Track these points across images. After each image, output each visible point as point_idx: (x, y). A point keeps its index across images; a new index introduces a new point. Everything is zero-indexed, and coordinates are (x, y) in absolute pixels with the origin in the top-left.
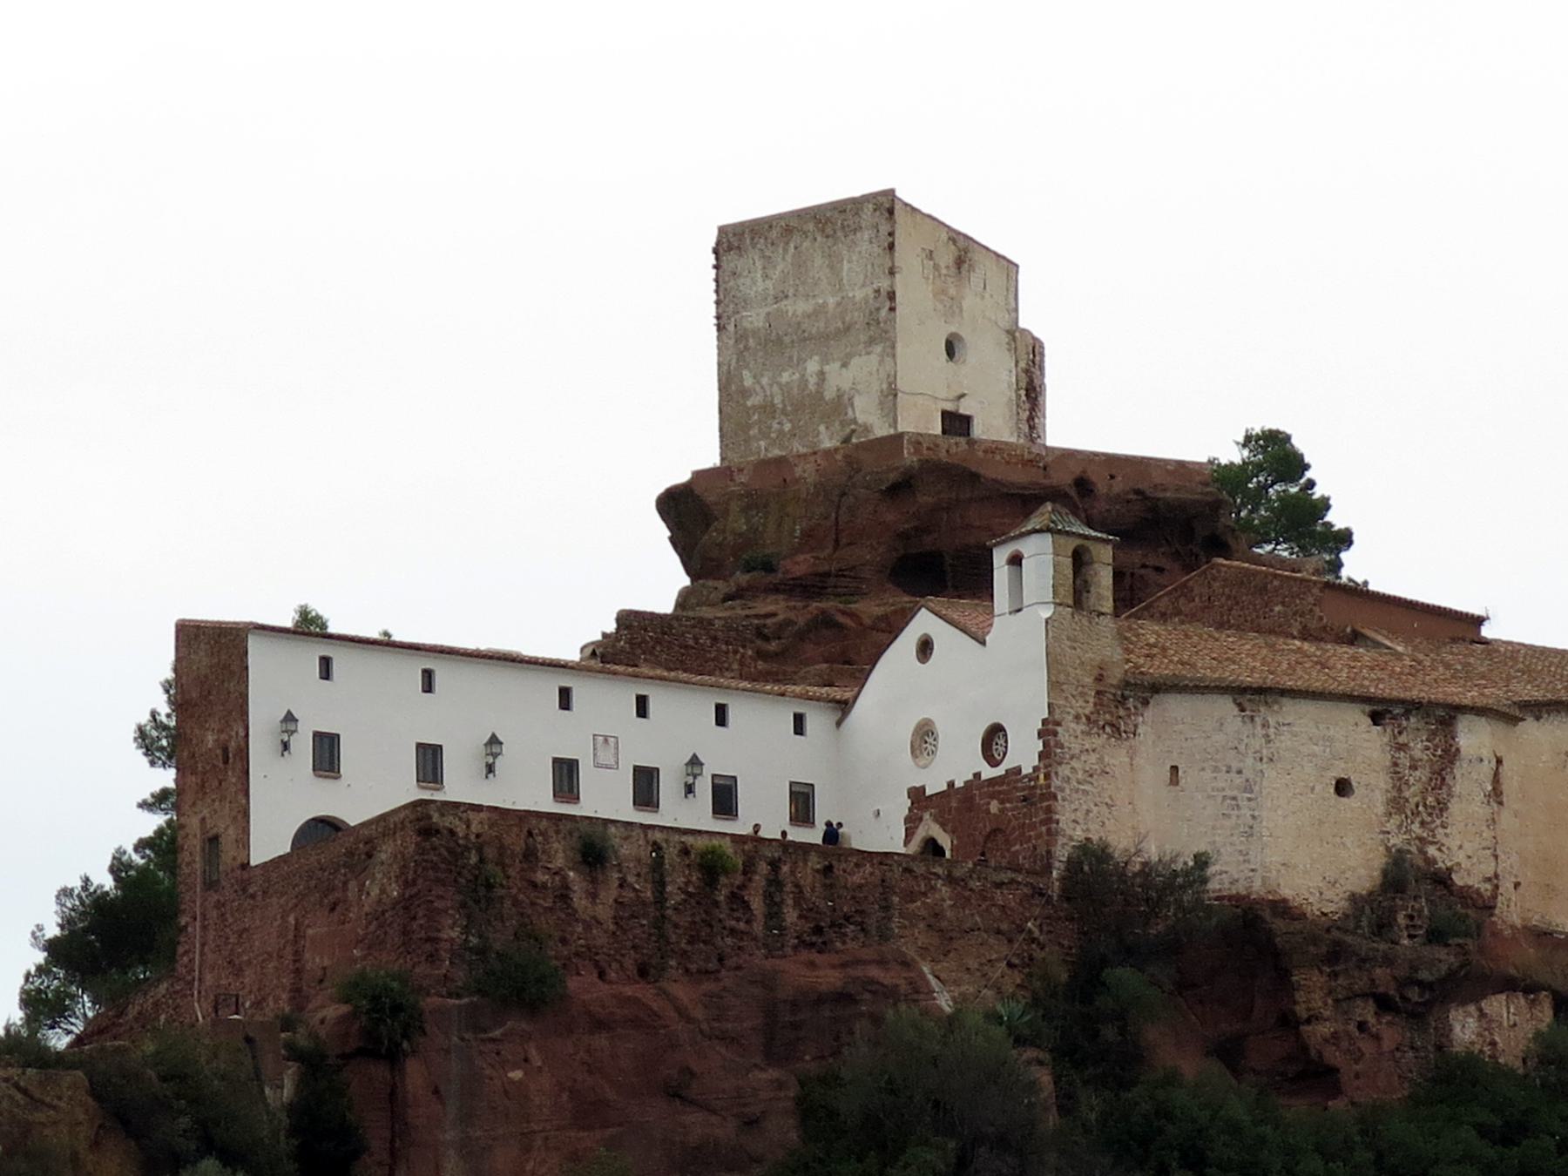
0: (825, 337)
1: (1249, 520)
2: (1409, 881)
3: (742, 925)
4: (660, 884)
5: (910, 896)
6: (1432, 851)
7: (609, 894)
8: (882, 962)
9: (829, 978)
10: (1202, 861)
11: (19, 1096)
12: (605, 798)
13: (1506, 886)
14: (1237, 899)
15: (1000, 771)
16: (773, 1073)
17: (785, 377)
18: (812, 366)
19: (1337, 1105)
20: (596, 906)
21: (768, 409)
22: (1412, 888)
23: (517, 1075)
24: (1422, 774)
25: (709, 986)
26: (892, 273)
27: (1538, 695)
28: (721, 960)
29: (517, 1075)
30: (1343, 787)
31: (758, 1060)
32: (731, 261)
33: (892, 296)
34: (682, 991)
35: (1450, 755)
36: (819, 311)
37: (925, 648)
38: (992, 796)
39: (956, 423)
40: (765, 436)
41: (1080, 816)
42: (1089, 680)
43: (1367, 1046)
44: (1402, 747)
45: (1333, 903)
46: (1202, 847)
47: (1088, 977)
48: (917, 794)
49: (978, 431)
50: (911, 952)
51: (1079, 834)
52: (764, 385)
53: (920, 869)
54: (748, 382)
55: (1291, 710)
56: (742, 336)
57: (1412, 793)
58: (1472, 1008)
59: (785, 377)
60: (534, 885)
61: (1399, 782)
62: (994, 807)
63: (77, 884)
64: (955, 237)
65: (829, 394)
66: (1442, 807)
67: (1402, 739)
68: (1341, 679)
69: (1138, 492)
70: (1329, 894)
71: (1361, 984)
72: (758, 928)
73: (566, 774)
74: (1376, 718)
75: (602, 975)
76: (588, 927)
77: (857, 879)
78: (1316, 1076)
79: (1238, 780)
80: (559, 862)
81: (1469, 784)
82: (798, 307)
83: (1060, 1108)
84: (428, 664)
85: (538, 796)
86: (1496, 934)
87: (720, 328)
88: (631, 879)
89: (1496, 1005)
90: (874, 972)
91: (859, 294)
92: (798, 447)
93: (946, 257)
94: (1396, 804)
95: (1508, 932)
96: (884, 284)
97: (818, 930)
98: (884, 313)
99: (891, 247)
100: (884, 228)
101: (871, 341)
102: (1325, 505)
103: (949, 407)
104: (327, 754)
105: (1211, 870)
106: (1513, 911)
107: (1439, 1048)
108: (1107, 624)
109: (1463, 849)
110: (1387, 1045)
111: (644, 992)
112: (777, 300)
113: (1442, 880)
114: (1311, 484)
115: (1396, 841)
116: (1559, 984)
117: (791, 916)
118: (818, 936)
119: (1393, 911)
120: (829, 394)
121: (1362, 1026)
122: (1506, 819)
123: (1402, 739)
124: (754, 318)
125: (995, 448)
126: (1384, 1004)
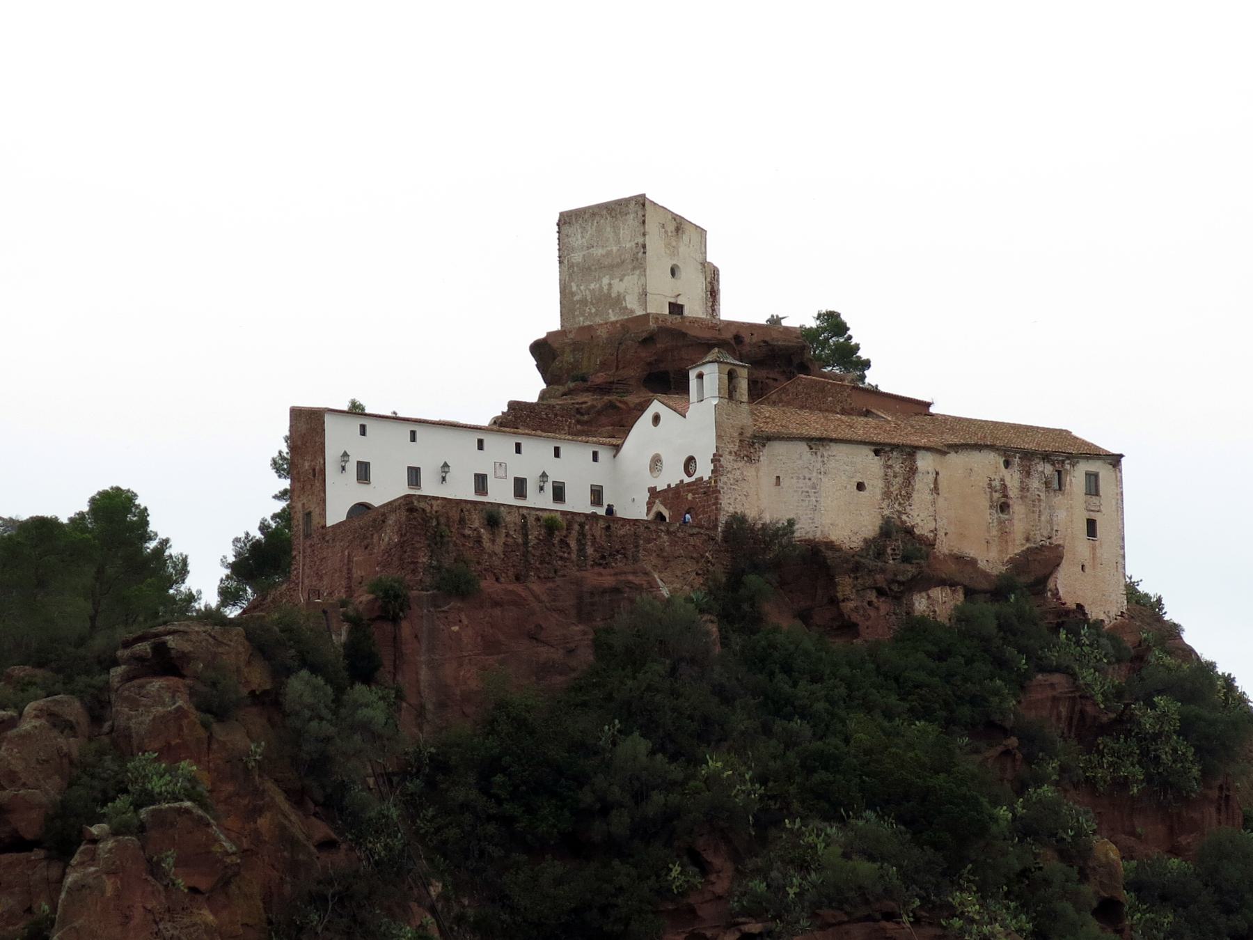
4: (526, 535)
5: (649, 541)
6: (904, 517)
7: (501, 540)
9: (608, 581)
10: (791, 523)
12: (500, 493)
13: (941, 533)
15: (693, 479)
16: (581, 627)
17: (592, 286)
18: (605, 281)
20: (494, 546)
21: (584, 302)
22: (894, 536)
23: (455, 628)
24: (899, 480)
26: (644, 235)
29: (455, 628)
30: (860, 487)
32: (566, 229)
33: (644, 246)
34: (536, 587)
35: (913, 471)
36: (609, 254)
37: (656, 419)
38: (689, 491)
39: (676, 308)
40: (583, 315)
42: (736, 435)
43: (872, 613)
44: (890, 467)
45: (856, 543)
47: (735, 580)
48: (652, 491)
49: (687, 312)
50: (649, 568)
51: (731, 510)
53: (653, 527)
54: (574, 288)
55: (836, 449)
56: (571, 266)
58: (924, 594)
59: (592, 286)
60: (464, 536)
62: (690, 496)
63: (242, 536)
66: (909, 496)
67: (890, 463)
68: (860, 433)
69: (765, 342)
70: (854, 539)
71: (869, 582)
72: (574, 556)
73: (481, 482)
74: (877, 453)
75: (497, 580)
76: (490, 556)
78: (849, 628)
79: (810, 483)
81: (922, 484)
82: (599, 252)
85: (467, 492)
88: (512, 533)
89: (936, 593)
90: (631, 578)
91: (628, 246)
92: (598, 320)
93: (671, 227)
94: (887, 494)
96: (641, 240)
97: (603, 557)
98: (640, 254)
99: (644, 222)
100: (640, 213)
101: (634, 269)
102: (857, 347)
103: (673, 300)
104: (364, 472)
105: (797, 527)
106: (944, 546)
107: (908, 613)
109: (920, 517)
110: (882, 612)
111: (518, 588)
112: (588, 248)
113: (909, 531)
115: (887, 512)
116: (966, 583)
117: (590, 550)
118: (603, 560)
119: (885, 547)
121: (870, 603)
123: (890, 463)
124: (577, 257)
125: (694, 321)
126: (881, 592)
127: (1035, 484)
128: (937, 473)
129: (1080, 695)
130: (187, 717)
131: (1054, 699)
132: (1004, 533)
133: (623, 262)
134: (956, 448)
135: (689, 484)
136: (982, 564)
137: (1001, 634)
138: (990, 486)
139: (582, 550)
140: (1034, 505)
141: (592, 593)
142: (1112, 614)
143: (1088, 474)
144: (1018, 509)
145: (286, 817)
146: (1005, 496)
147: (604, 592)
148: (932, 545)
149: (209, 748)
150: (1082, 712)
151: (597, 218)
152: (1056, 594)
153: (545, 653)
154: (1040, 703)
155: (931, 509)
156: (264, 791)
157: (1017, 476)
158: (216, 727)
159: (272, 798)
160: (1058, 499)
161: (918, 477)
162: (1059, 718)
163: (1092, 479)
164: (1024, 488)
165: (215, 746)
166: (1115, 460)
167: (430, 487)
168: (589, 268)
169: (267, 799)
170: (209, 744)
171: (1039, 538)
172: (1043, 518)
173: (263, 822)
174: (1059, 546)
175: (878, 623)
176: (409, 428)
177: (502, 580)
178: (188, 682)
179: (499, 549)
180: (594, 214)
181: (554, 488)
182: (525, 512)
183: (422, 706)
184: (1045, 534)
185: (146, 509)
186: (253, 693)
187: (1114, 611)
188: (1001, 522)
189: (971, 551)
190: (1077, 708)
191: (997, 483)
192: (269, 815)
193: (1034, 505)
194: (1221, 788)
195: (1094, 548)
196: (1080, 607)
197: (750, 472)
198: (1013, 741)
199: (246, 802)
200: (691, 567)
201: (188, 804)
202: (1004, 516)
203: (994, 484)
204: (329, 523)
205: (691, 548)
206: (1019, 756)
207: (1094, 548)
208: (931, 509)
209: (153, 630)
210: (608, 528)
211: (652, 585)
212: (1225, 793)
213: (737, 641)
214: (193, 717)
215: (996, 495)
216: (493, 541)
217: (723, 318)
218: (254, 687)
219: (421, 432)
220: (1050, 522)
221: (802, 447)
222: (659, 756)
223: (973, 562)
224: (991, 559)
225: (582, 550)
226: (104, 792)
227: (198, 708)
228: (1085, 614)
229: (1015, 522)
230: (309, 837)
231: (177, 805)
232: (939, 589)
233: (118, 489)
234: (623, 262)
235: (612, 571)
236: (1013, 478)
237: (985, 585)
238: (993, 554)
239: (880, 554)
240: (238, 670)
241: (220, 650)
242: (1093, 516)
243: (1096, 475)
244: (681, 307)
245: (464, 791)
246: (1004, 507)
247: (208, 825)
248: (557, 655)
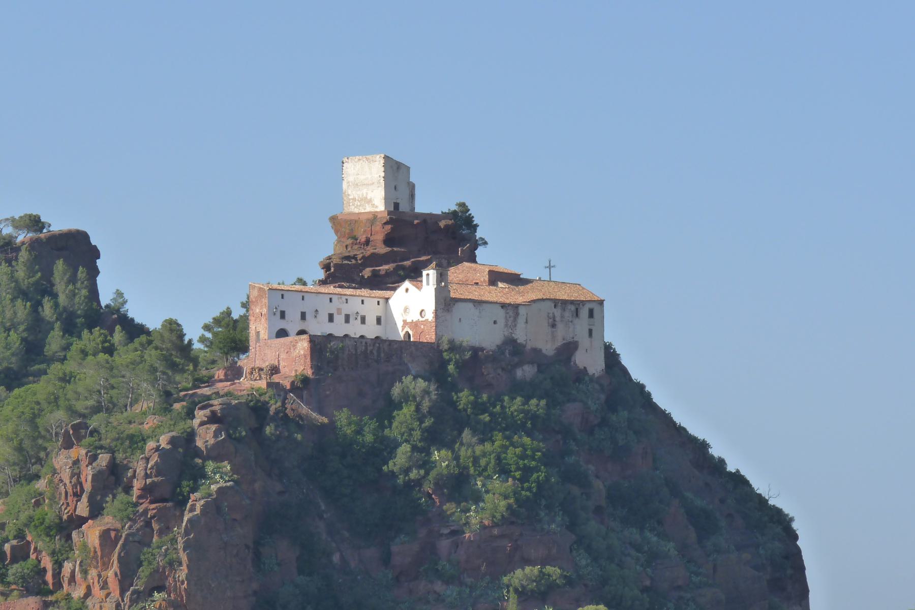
0: (368, 185)
1: (539, 400)
2: (510, 342)
4: (356, 350)
21: (354, 199)
30: (495, 322)
37: (407, 290)
45: (494, 347)
55: (484, 305)
64: (397, 163)
66: (515, 326)
82: (362, 177)
94: (506, 325)
109: (520, 335)
115: (506, 333)
117: (382, 355)
126: (503, 369)
127: (567, 314)
132: (554, 337)
136: (544, 351)
139: (379, 355)
148: (524, 346)
152: (575, 363)
160: (576, 321)
163: (591, 314)
164: (562, 317)
166: (601, 303)
171: (569, 339)
174: (577, 342)
176: (301, 294)
191: (551, 315)
215: (551, 320)
217: (416, 211)
219: (306, 295)
221: (471, 305)
223: (540, 350)
225: (379, 355)
236: (558, 312)
239: (503, 353)
242: (591, 327)
246: (553, 326)
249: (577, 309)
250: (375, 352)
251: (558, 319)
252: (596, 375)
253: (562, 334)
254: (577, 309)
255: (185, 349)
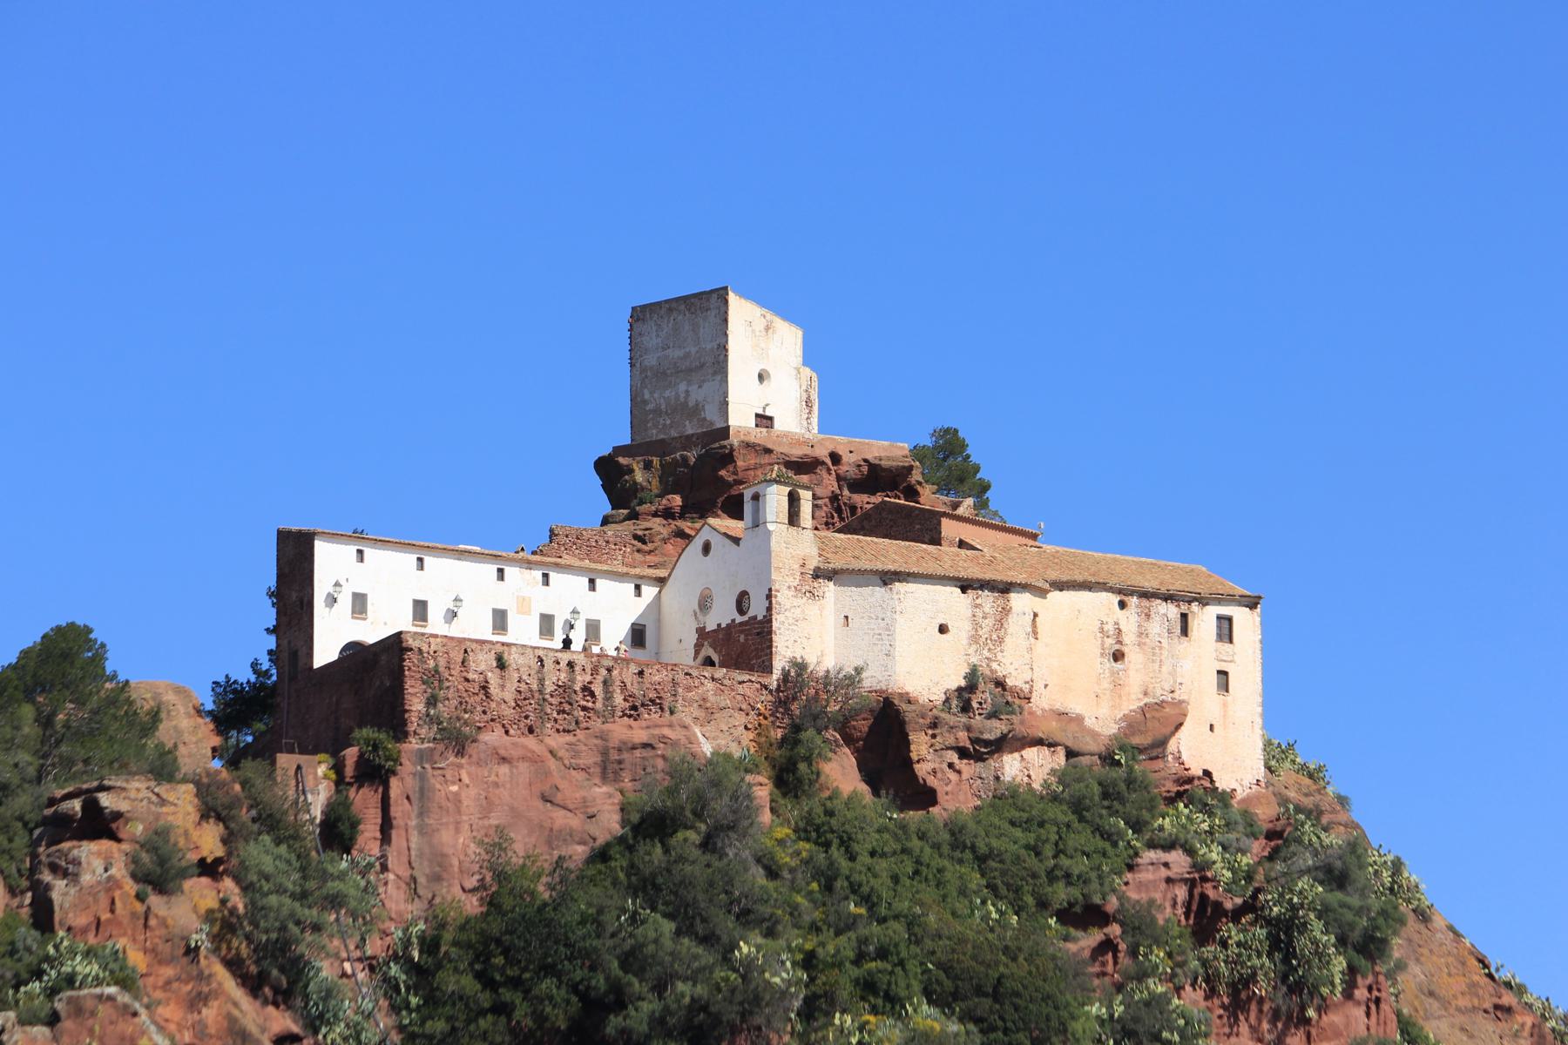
0: (690, 370)
3: (590, 705)
4: (541, 681)
5: (689, 689)
6: (994, 666)
7: (512, 686)
8: (671, 726)
9: (640, 735)
10: (858, 670)
11: (154, 798)
12: (523, 631)
13: (1039, 686)
14: (879, 692)
15: (745, 618)
16: (605, 789)
17: (667, 394)
18: (682, 387)
19: (934, 810)
20: (504, 692)
21: (657, 411)
22: (981, 686)
23: (454, 788)
24: (989, 622)
25: (569, 738)
27: (1065, 578)
28: (577, 723)
29: (454, 788)
30: (943, 629)
31: (597, 781)
32: (638, 327)
34: (557, 741)
35: (1006, 611)
36: (687, 355)
37: (706, 548)
38: (742, 632)
39: (764, 420)
40: (655, 426)
41: (789, 644)
42: (796, 566)
43: (953, 776)
44: (977, 606)
46: (860, 663)
47: (792, 738)
48: (701, 632)
49: (778, 425)
50: (688, 721)
51: (789, 654)
52: (657, 398)
53: (695, 673)
54: (647, 396)
56: (643, 370)
57: (984, 633)
58: (1016, 755)
59: (667, 394)
60: (467, 680)
61: (976, 626)
62: (742, 638)
63: (222, 679)
65: (691, 404)
66: (1001, 640)
67: (979, 601)
68: (946, 568)
69: (865, 460)
70: (934, 690)
71: (951, 741)
72: (599, 705)
73: (500, 620)
74: (964, 590)
75: (507, 732)
76: (499, 704)
77: (657, 678)
78: (926, 797)
79: (883, 624)
80: (482, 667)
81: (1017, 625)
82: (677, 353)
83: (772, 809)
84: (1184, 608)
85: (484, 631)
86: (1031, 713)
87: (632, 365)
88: (525, 677)
89: (1031, 753)
90: (666, 731)
91: (709, 346)
92: (674, 434)
94: (975, 639)
95: (1039, 713)
97: (634, 708)
101: (715, 373)
102: (977, 469)
103: (760, 412)
104: (360, 604)
105: (864, 675)
106: (1042, 701)
107: (997, 778)
108: (809, 534)
109: (1013, 666)
110: (965, 776)
111: (530, 742)
112: (664, 349)
113: (1000, 684)
114: (968, 456)
115: (974, 660)
116: (1069, 744)
117: (618, 699)
118: (633, 711)
119: (969, 700)
120: (691, 404)
121: (951, 766)
122: (1039, 647)
123: (979, 601)
124: (651, 360)
125: (786, 435)
126: (963, 753)
127: (1155, 628)
128: (1035, 615)
129: (1200, 873)
130: (120, 888)
131: (1169, 880)
132: (1117, 685)
133: (702, 366)
134: (1060, 586)
135: (741, 624)
136: (1089, 722)
137: (1106, 803)
138: (1102, 631)
139: (608, 697)
140: (1154, 654)
141: (620, 750)
142: (1246, 783)
143: (1219, 618)
144: (1133, 656)
145: (236, 1004)
146: (1120, 642)
147: (634, 748)
149: (146, 926)
150: (1203, 897)
151: (675, 314)
152: (1178, 758)
153: (561, 818)
154: (1152, 883)
155: (1027, 656)
156: (210, 976)
157: (1134, 619)
158: (154, 900)
159: (220, 984)
161: (1012, 619)
162: (1174, 905)
165: (153, 922)
167: (436, 624)
168: (664, 373)
169: (214, 985)
170: (146, 919)
171: (1159, 693)
172: (1164, 669)
173: (210, 1014)
174: (1181, 702)
175: (959, 792)
177: (512, 732)
178: (125, 847)
179: (509, 695)
180: (670, 310)
181: (588, 626)
182: (541, 653)
183: (414, 880)
184: (1167, 687)
185: (103, 646)
186: (202, 861)
187: (1249, 779)
188: (1113, 673)
189: (1075, 706)
190: (1197, 891)
191: (1110, 628)
192: (216, 1004)
193: (1154, 654)
194: (1370, 989)
195: (1225, 705)
196: (1207, 773)
197: (812, 608)
198: (1115, 930)
199: (189, 987)
200: (740, 719)
201: (112, 990)
202: (1118, 666)
203: (1106, 628)
204: (316, 665)
205: (740, 698)
206: (1123, 946)
207: (1225, 705)
208: (1027, 656)
209: (85, 786)
210: (641, 673)
211: (691, 740)
212: (1375, 993)
213: (794, 813)
214: (127, 888)
216: (503, 687)
218: (205, 853)
220: (1173, 674)
222: (686, 941)
223: (1079, 719)
224: (1101, 714)
226: (16, 975)
227: (134, 876)
228: (1212, 781)
229: (1132, 673)
230: (263, 1030)
231: (98, 990)
232: (1035, 749)
233: (73, 624)
234: (702, 366)
235: (644, 724)
237: (1092, 746)
238: (1104, 710)
240: (186, 833)
241: (164, 809)
243: (1230, 620)
244: (771, 419)
245: (458, 981)
246: (1118, 656)
247: (135, 1014)
248: (575, 822)
249: (1184, 616)
250: (598, 689)
251: (1129, 638)
252: (1240, 795)
253: (1140, 681)
254: (1184, 616)
255: (1084, 1005)
